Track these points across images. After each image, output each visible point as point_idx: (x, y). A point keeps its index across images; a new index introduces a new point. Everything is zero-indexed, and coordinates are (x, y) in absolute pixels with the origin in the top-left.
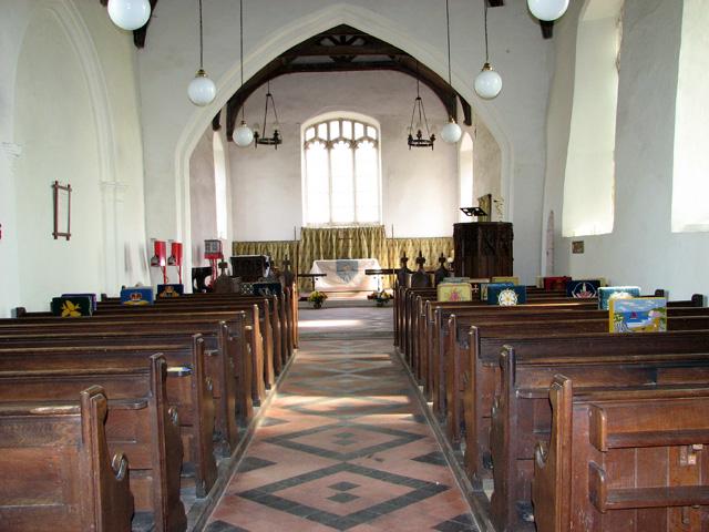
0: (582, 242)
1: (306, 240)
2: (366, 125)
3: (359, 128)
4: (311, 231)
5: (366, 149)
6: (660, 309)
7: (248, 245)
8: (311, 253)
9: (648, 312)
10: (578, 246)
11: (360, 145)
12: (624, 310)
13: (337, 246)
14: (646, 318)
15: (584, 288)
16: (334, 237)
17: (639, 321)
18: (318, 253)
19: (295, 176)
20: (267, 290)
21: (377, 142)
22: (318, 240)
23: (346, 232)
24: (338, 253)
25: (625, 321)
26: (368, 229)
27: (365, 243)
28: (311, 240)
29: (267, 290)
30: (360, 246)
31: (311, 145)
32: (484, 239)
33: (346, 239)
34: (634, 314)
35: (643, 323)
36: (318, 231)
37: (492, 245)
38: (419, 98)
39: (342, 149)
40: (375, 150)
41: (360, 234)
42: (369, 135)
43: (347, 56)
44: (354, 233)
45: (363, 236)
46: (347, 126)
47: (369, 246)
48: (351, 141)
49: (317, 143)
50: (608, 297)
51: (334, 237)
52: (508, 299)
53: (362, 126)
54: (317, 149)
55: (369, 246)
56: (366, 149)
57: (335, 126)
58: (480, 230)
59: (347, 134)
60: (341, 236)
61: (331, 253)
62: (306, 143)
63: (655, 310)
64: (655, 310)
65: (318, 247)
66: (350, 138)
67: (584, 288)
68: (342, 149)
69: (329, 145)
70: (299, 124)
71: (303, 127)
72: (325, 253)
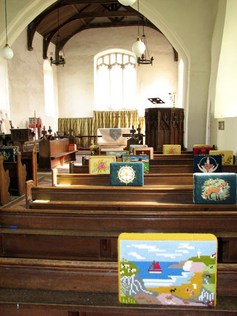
0: (223, 122)
1: (96, 118)
2: (130, 56)
3: (126, 58)
4: (99, 112)
5: (129, 68)
6: (205, 259)
7: (66, 120)
8: (99, 124)
9: (183, 263)
10: (221, 125)
11: (126, 67)
12: (139, 258)
13: (113, 121)
14: (179, 272)
15: (208, 161)
16: (111, 116)
17: (164, 277)
18: (103, 124)
19: (91, 84)
20: (4, 153)
21: (135, 65)
22: (102, 118)
23: (117, 113)
24: (113, 125)
25: (140, 277)
26: (129, 112)
27: (127, 120)
28: (99, 117)
29: (4, 153)
30: (125, 121)
31: (100, 67)
32: (162, 119)
33: (117, 117)
34: (156, 266)
35: (173, 281)
36: (102, 113)
37: (168, 122)
38: (144, 36)
39: (116, 68)
40: (134, 69)
41: (124, 114)
42: (131, 62)
43: (120, 17)
44: (122, 114)
45: (126, 116)
46: (120, 56)
47: (129, 121)
48: (122, 65)
49: (104, 66)
50: (202, 184)
51: (111, 116)
52: (126, 175)
53: (127, 57)
54: (104, 68)
55: (129, 121)
56: (129, 68)
57: (113, 56)
58: (159, 113)
59: (107, 61)
60: (114, 115)
61: (109, 124)
62: (97, 66)
63: (195, 259)
64: (195, 259)
65: (103, 121)
66: (121, 63)
67: (208, 161)
68: (116, 68)
69: (110, 67)
70: (93, 56)
71: (96, 57)
72: (106, 125)
